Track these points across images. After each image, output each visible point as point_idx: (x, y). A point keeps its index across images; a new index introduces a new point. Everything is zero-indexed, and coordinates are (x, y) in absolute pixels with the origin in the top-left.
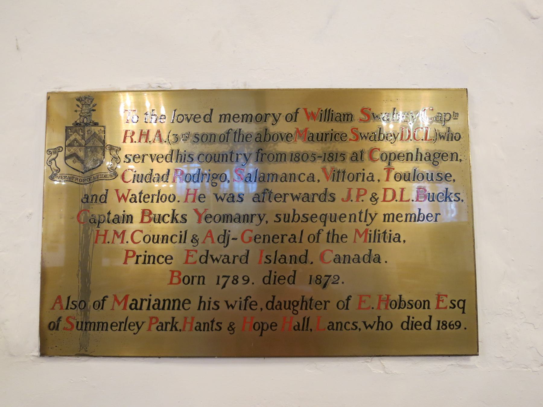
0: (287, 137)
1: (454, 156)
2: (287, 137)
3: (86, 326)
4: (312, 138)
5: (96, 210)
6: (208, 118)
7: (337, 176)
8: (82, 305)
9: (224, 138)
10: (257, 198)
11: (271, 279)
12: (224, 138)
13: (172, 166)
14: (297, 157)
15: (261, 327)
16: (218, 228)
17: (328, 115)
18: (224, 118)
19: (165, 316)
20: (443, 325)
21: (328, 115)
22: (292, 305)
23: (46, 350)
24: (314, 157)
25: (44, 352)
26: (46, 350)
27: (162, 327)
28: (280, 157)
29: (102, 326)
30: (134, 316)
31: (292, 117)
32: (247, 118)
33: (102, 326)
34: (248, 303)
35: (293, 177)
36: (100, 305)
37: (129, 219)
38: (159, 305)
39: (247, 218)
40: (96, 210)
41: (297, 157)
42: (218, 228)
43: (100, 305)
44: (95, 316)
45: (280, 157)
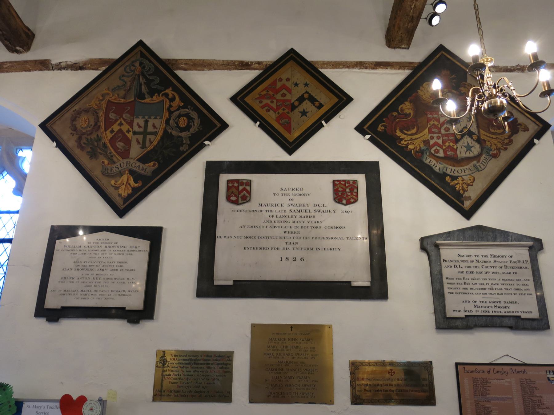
0: (200, 360)
1: (230, 364)
2: (200, 360)
3: (161, 395)
4: (204, 360)
5: (165, 373)
6: (186, 356)
7: (208, 368)
8: (161, 391)
9: (188, 360)
10: (194, 372)
11: (195, 387)
12: (188, 360)
13: (179, 365)
14: (201, 364)
15: (193, 396)
16: (186, 377)
17: (208, 356)
18: (189, 356)
19: (176, 394)
20: (226, 396)
21: (208, 356)
22: (199, 392)
23: (154, 400)
24: (204, 364)
25: (153, 400)
26: (154, 400)
27: (175, 396)
28: (198, 364)
29: (164, 395)
30: (170, 394)
31: (201, 356)
32: (193, 356)
33: (164, 395)
34: (191, 392)
35: (200, 368)
36: (164, 391)
37: (170, 375)
38: (175, 392)
39: (192, 375)
40: (165, 373)
41: (201, 364)
42: (186, 377)
43: (164, 391)
44: (163, 394)
45: (198, 364)
